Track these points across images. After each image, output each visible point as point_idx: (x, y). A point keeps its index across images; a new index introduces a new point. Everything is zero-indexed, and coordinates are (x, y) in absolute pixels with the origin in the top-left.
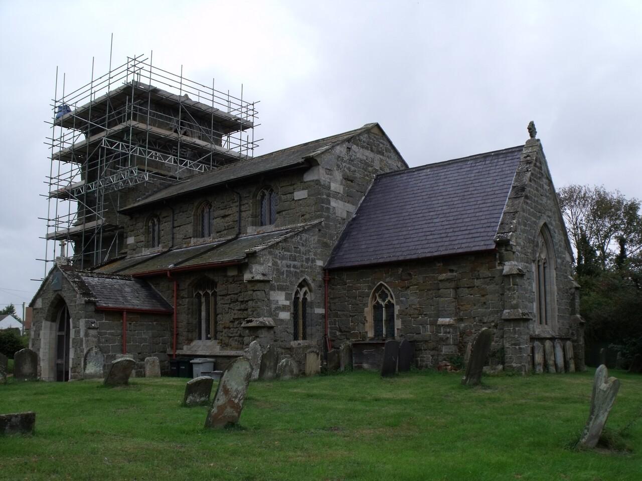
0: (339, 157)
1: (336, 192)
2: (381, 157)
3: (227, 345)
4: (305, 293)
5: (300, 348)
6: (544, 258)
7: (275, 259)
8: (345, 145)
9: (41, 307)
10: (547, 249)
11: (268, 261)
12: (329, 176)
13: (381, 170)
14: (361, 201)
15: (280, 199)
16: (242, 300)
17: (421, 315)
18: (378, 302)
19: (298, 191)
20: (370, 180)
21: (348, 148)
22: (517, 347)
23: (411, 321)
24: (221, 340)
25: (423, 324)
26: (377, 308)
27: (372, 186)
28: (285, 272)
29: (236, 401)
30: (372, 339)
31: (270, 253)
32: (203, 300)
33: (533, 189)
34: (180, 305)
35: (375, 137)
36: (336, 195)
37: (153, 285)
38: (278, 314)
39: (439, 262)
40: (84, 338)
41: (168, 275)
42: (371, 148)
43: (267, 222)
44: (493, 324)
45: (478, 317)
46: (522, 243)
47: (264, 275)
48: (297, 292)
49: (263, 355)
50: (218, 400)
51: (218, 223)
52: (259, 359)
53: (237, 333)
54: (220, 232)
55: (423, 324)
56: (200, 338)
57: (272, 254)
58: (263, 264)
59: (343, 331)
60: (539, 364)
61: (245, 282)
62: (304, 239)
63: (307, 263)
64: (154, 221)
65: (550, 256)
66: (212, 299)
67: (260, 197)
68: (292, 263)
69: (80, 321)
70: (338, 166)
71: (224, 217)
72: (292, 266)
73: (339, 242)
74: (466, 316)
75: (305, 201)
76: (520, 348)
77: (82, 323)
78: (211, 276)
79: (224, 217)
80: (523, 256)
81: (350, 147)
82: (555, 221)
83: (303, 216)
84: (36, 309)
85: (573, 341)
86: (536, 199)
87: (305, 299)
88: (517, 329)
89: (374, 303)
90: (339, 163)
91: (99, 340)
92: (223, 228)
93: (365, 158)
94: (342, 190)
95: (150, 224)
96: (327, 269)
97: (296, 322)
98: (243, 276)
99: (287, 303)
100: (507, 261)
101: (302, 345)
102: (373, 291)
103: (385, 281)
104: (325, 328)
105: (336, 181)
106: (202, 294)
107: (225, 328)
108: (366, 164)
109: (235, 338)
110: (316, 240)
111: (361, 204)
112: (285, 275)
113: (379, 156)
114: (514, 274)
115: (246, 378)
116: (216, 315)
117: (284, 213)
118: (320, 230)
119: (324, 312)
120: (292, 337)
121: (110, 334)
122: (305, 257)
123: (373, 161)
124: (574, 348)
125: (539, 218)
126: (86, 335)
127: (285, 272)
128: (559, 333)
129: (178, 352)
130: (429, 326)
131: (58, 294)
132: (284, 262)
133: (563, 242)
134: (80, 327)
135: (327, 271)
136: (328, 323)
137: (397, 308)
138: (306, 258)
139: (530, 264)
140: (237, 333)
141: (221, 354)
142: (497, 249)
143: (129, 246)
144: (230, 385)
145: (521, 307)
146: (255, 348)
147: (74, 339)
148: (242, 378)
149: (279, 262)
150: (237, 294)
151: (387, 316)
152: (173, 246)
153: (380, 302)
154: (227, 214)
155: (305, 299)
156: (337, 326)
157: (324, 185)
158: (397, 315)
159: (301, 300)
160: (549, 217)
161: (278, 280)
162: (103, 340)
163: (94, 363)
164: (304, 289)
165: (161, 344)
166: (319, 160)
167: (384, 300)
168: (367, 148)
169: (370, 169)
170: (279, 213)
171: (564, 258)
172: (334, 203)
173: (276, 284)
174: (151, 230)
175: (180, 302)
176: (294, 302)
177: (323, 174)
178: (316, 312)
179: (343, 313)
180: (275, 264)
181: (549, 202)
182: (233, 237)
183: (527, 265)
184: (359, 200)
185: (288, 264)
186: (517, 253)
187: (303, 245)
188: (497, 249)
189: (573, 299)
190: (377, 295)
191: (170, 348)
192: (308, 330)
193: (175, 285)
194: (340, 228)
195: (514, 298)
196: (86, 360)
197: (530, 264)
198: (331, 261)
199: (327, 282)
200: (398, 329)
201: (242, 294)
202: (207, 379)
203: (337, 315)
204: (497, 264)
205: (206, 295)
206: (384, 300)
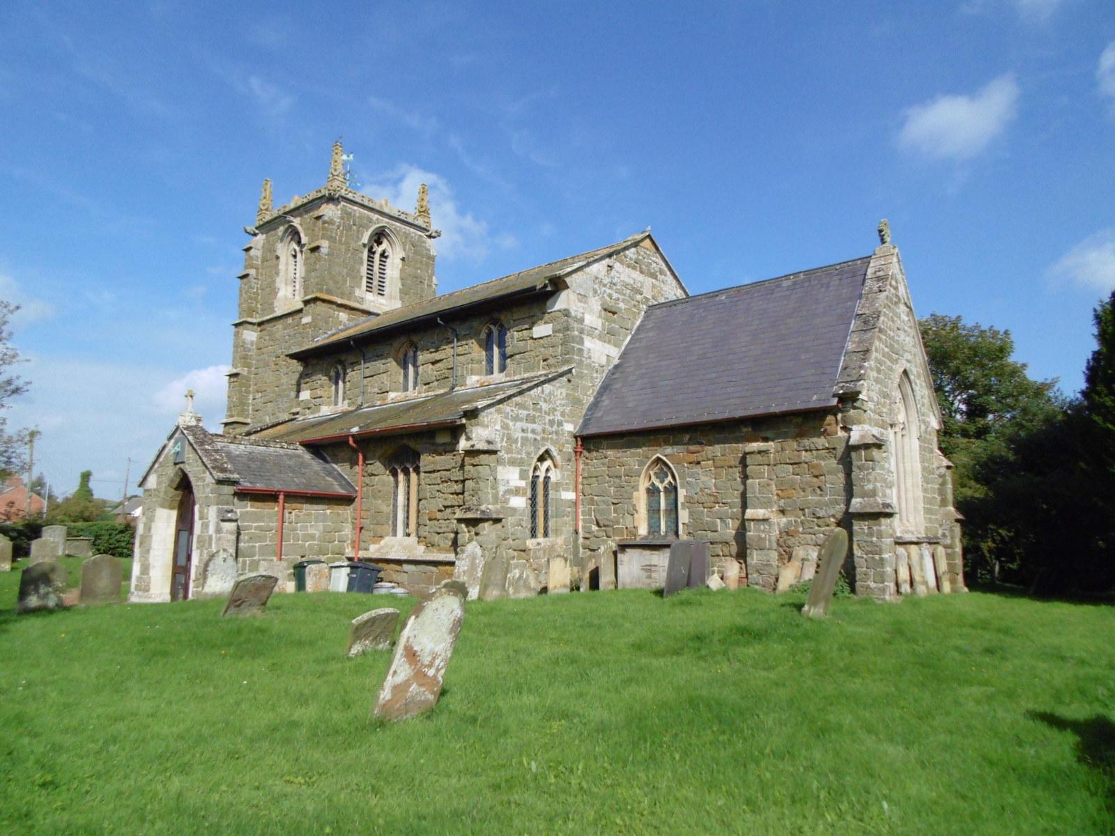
0: (597, 278)
1: (591, 327)
2: (654, 281)
4: (548, 470)
5: (539, 550)
6: (902, 421)
7: (505, 421)
8: (607, 261)
9: (155, 487)
10: (906, 409)
11: (495, 423)
12: (582, 305)
13: (653, 298)
14: (626, 342)
17: (718, 503)
18: (653, 483)
20: (639, 313)
21: (608, 266)
22: (877, 557)
23: (703, 512)
26: (652, 492)
27: (642, 322)
28: (520, 439)
29: (431, 672)
30: (645, 538)
31: (498, 411)
33: (888, 318)
35: (645, 253)
36: (591, 332)
38: (509, 499)
39: (746, 426)
40: (214, 535)
42: (640, 268)
45: (808, 508)
46: (875, 399)
47: (489, 442)
48: (535, 469)
49: (485, 564)
50: (395, 672)
51: (428, 371)
52: (479, 569)
54: (428, 384)
56: (395, 534)
57: (501, 413)
58: (488, 426)
59: (601, 525)
60: (905, 581)
61: (461, 452)
63: (552, 427)
64: (337, 369)
65: (910, 419)
67: (485, 335)
68: (531, 426)
69: (210, 508)
70: (595, 291)
71: (433, 363)
72: (529, 430)
73: (596, 398)
74: (790, 506)
75: (549, 339)
76: (882, 559)
77: (212, 513)
78: (412, 444)
80: (877, 417)
81: (611, 264)
82: (916, 366)
83: (544, 361)
84: (147, 490)
85: (946, 547)
86: (892, 334)
87: (547, 478)
88: (875, 528)
89: (647, 484)
90: (596, 286)
92: (434, 378)
93: (632, 282)
94: (600, 324)
96: (580, 436)
97: (535, 512)
99: (523, 484)
100: (855, 424)
101: (543, 545)
102: (645, 468)
103: (665, 452)
104: (576, 519)
105: (592, 312)
107: (430, 520)
108: (633, 289)
110: (564, 394)
111: (627, 346)
112: (519, 443)
113: (650, 280)
114: (192, 426)
115: (452, 628)
117: (517, 356)
118: (569, 381)
119: (574, 498)
120: (528, 532)
121: (256, 528)
122: (548, 418)
124: (949, 556)
125: (896, 361)
126: (218, 530)
127: (520, 439)
128: (926, 534)
131: (180, 469)
133: (927, 398)
134: (210, 519)
136: (580, 514)
137: (682, 493)
138: (549, 420)
139: (886, 429)
142: (840, 405)
144: (420, 644)
145: (880, 494)
146: (473, 553)
147: (199, 537)
148: (444, 630)
149: (511, 424)
151: (667, 505)
153: (657, 483)
154: (438, 359)
155: (547, 478)
156: (593, 517)
157: (576, 317)
158: (682, 503)
160: (908, 361)
161: (509, 451)
162: (246, 537)
163: (220, 576)
164: (548, 463)
165: (336, 542)
166: (568, 280)
167: (662, 482)
168: (634, 268)
169: (639, 297)
171: (929, 423)
172: (589, 343)
173: (506, 456)
176: (532, 482)
177: (575, 301)
178: (563, 498)
179: (602, 498)
180: (505, 427)
181: (907, 339)
182: (446, 390)
183: (883, 430)
184: (623, 340)
185: (524, 428)
186: (869, 412)
187: (545, 401)
188: (840, 405)
189: (943, 484)
191: (350, 549)
192: (551, 523)
194: (597, 378)
195: (869, 481)
197: (886, 429)
198: (586, 423)
199: (578, 454)
200: (683, 524)
202: (388, 614)
206: (662, 482)
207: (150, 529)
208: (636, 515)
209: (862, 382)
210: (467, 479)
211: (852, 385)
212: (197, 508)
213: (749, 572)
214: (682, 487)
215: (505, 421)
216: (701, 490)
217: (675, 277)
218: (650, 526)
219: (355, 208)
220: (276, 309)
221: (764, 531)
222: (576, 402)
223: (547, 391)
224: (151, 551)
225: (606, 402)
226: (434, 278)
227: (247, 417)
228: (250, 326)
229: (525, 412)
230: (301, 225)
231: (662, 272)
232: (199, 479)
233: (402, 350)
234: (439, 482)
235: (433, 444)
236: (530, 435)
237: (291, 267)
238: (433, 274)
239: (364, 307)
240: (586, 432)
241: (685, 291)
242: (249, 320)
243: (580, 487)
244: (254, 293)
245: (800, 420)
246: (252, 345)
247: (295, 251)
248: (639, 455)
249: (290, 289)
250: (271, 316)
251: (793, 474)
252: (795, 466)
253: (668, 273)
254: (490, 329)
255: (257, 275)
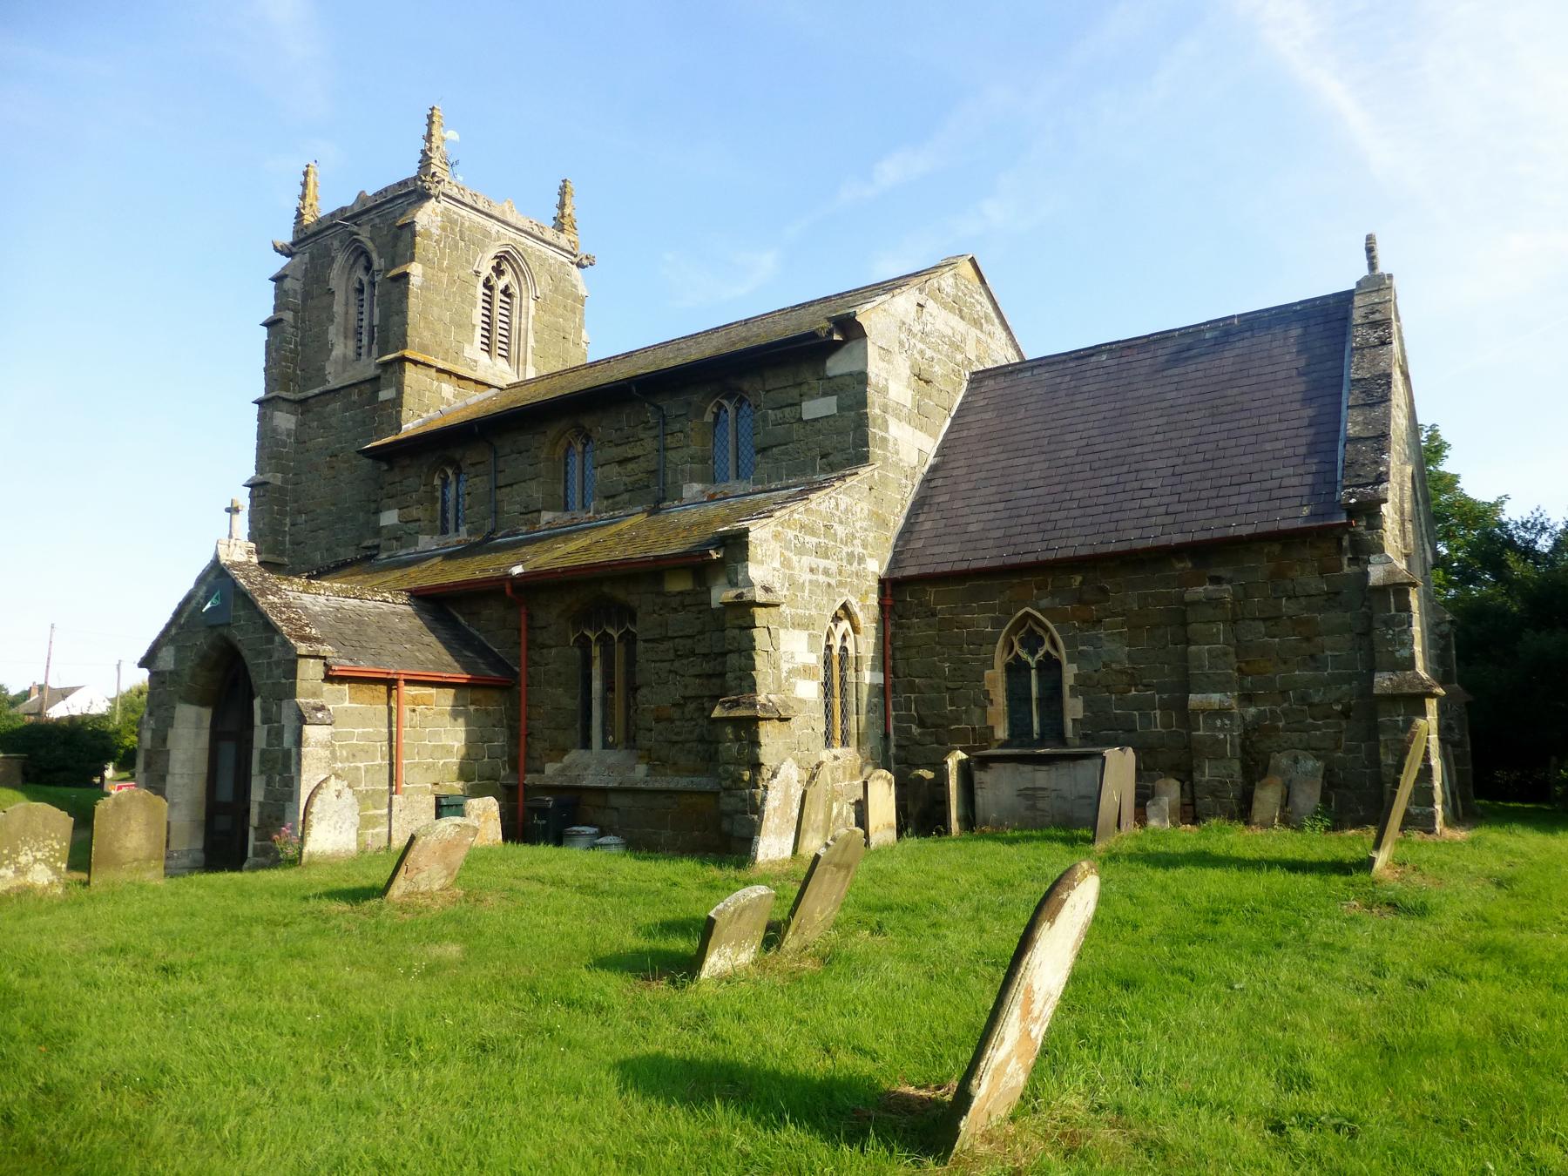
3: (664, 763)
7: (787, 553)
14: (944, 430)
15: (765, 418)
16: (706, 651)
19: (812, 398)
23: (1109, 701)
24: (649, 750)
25: (1144, 706)
26: (1016, 670)
32: (596, 651)
34: (536, 664)
37: (464, 615)
39: (1181, 560)
41: (508, 590)
43: (732, 472)
44: (1338, 708)
53: (691, 732)
54: (613, 496)
55: (1144, 706)
56: (586, 744)
62: (842, 507)
66: (619, 652)
68: (823, 563)
70: (901, 344)
71: (622, 462)
73: (908, 518)
78: (620, 594)
79: (622, 462)
90: (903, 336)
91: (333, 753)
93: (950, 333)
95: (437, 482)
98: (709, 591)
106: (593, 638)
107: (658, 720)
109: (688, 745)
113: (974, 332)
116: (632, 689)
122: (845, 549)
123: (963, 340)
129: (529, 779)
130: (1158, 712)
132: (804, 558)
135: (888, 585)
137: (1070, 672)
140: (691, 732)
141: (651, 786)
143: (384, 531)
149: (795, 559)
150: (689, 637)
152: (494, 531)
153: (1024, 655)
159: (836, 651)
167: (1033, 653)
168: (952, 310)
169: (959, 357)
170: (762, 450)
174: (438, 494)
175: (536, 658)
180: (786, 563)
187: (841, 522)
190: (1015, 640)
193: (523, 617)
196: (1260, 869)
198: (896, 561)
201: (707, 635)
203: (911, 687)
204: (1345, 561)
205: (605, 640)
206: (1033, 653)
207: (164, 740)
208: (990, 709)
209: (1385, 485)
210: (731, 651)
211: (1369, 490)
212: (257, 703)
213: (1198, 794)
214: (1070, 661)
215: (787, 553)
216: (1105, 665)
217: (1006, 328)
218: (1013, 725)
219: (464, 213)
220: (330, 378)
221: (1221, 729)
222: (883, 524)
223: (842, 507)
224: (169, 778)
225: (926, 525)
226: (584, 333)
227: (282, 554)
228: (285, 406)
229: (814, 540)
230: (371, 239)
231: (987, 317)
232: (259, 654)
233: (563, 442)
234: (671, 655)
235: (661, 594)
236: (822, 578)
237: (353, 311)
238: (581, 326)
239: (478, 375)
240: (898, 574)
241: (1019, 351)
242: (284, 394)
243: (890, 663)
244: (291, 351)
245: (1276, 548)
246: (289, 436)
247: (360, 282)
248: (992, 609)
249: (352, 344)
250: (321, 389)
251: (1266, 635)
252: (1269, 623)
253: (996, 321)
254: (720, 406)
255: (296, 321)
